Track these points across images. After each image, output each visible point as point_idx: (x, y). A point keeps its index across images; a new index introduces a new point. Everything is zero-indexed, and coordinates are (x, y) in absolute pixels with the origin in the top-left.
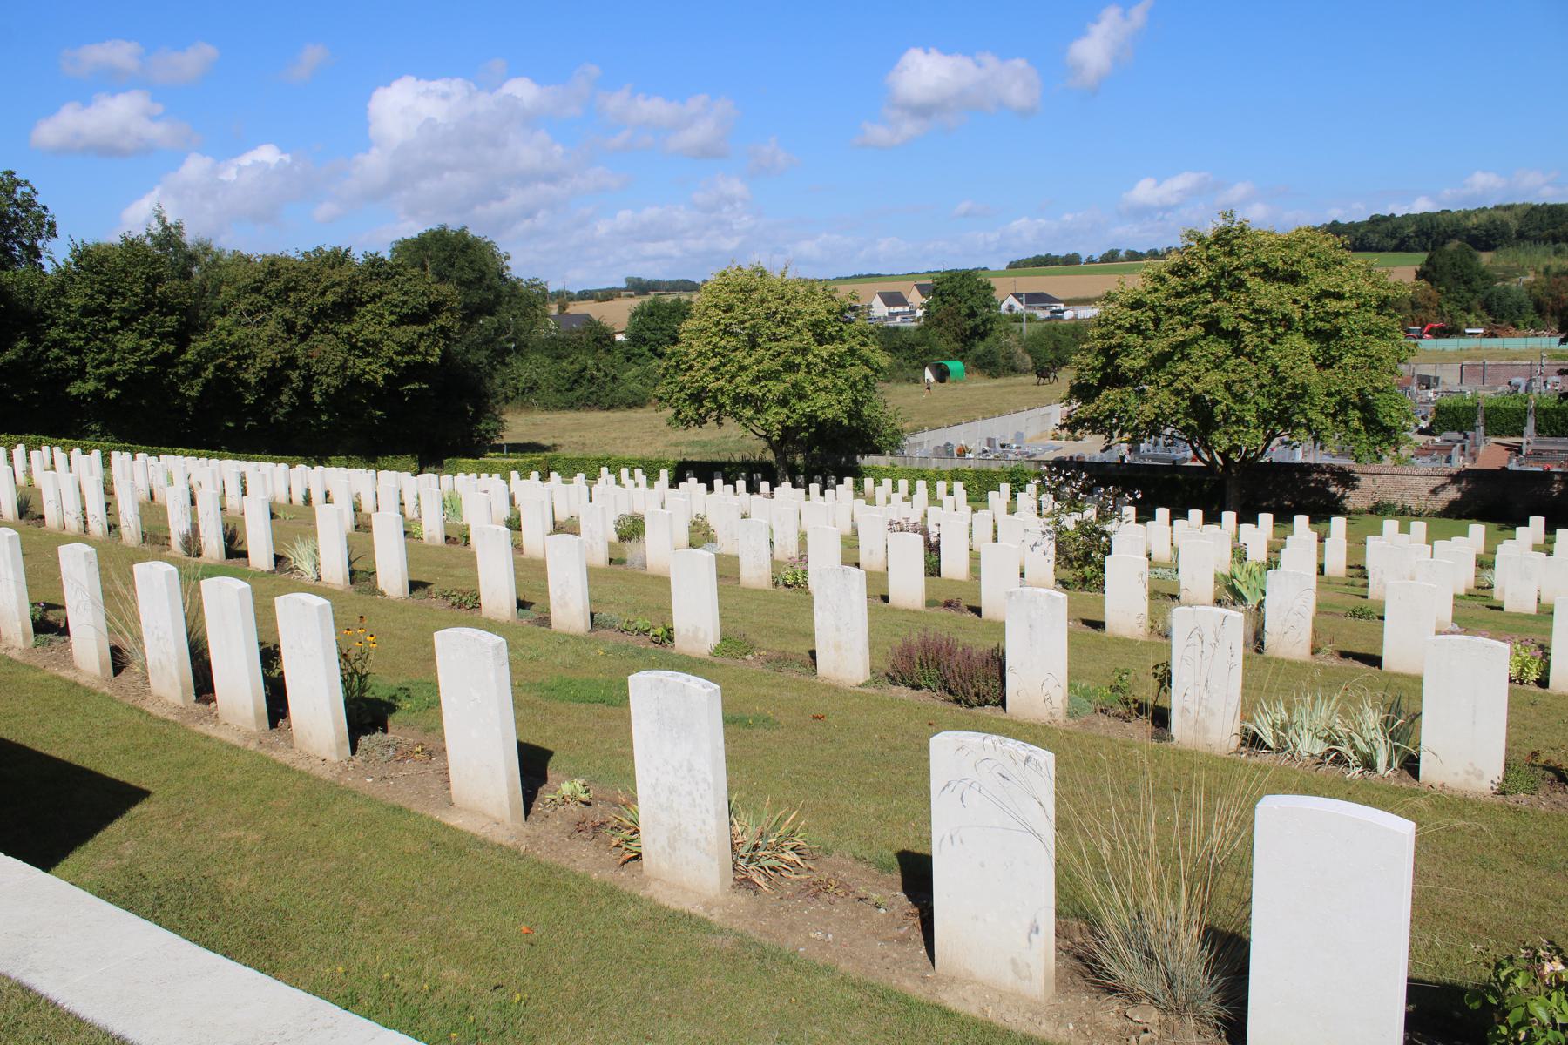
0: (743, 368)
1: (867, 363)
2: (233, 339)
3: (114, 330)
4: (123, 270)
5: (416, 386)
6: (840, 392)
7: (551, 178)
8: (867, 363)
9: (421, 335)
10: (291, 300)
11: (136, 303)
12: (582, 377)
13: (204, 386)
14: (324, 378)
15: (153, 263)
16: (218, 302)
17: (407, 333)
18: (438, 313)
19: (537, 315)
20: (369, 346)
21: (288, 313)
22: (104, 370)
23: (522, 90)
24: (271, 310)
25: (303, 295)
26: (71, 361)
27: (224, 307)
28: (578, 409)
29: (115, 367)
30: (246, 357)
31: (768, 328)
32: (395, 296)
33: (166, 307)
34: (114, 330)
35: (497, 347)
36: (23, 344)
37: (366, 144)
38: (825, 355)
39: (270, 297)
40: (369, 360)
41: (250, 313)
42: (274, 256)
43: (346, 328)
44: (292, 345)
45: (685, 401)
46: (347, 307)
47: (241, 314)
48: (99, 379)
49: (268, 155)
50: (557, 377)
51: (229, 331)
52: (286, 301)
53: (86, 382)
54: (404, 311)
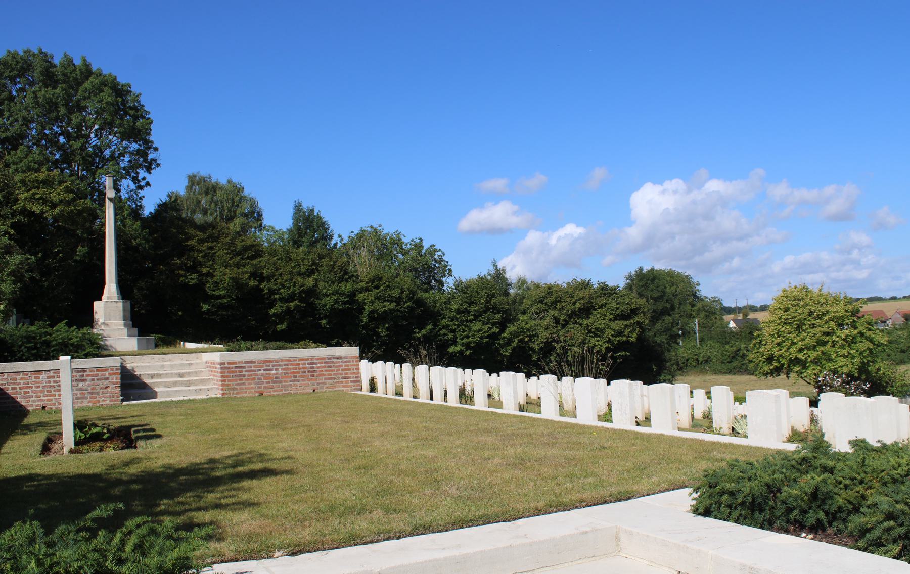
0: (794, 343)
1: (872, 341)
2: (528, 326)
3: (471, 321)
4: (477, 292)
5: (623, 353)
6: (853, 358)
7: (740, 239)
8: (872, 341)
9: (626, 326)
10: (557, 307)
11: (482, 308)
12: (737, 355)
13: (512, 350)
14: (573, 348)
15: (491, 288)
16: (521, 308)
17: (619, 325)
18: (636, 314)
19: (716, 318)
20: (598, 331)
21: (556, 313)
22: (465, 340)
23: (715, 186)
24: (548, 312)
25: (564, 304)
26: (451, 335)
27: (524, 310)
28: (734, 374)
29: (470, 339)
30: (534, 336)
31: (810, 321)
32: (613, 305)
33: (496, 309)
34: (471, 321)
35: (672, 334)
36: (430, 327)
37: (631, 223)
38: (843, 336)
39: (548, 305)
40: (598, 339)
41: (537, 313)
42: (550, 284)
43: (585, 322)
44: (557, 330)
45: (764, 362)
46: (587, 311)
47: (533, 314)
48: (462, 345)
49: (571, 230)
50: (722, 354)
51: (526, 322)
52: (555, 307)
53: (456, 346)
54: (617, 313)
